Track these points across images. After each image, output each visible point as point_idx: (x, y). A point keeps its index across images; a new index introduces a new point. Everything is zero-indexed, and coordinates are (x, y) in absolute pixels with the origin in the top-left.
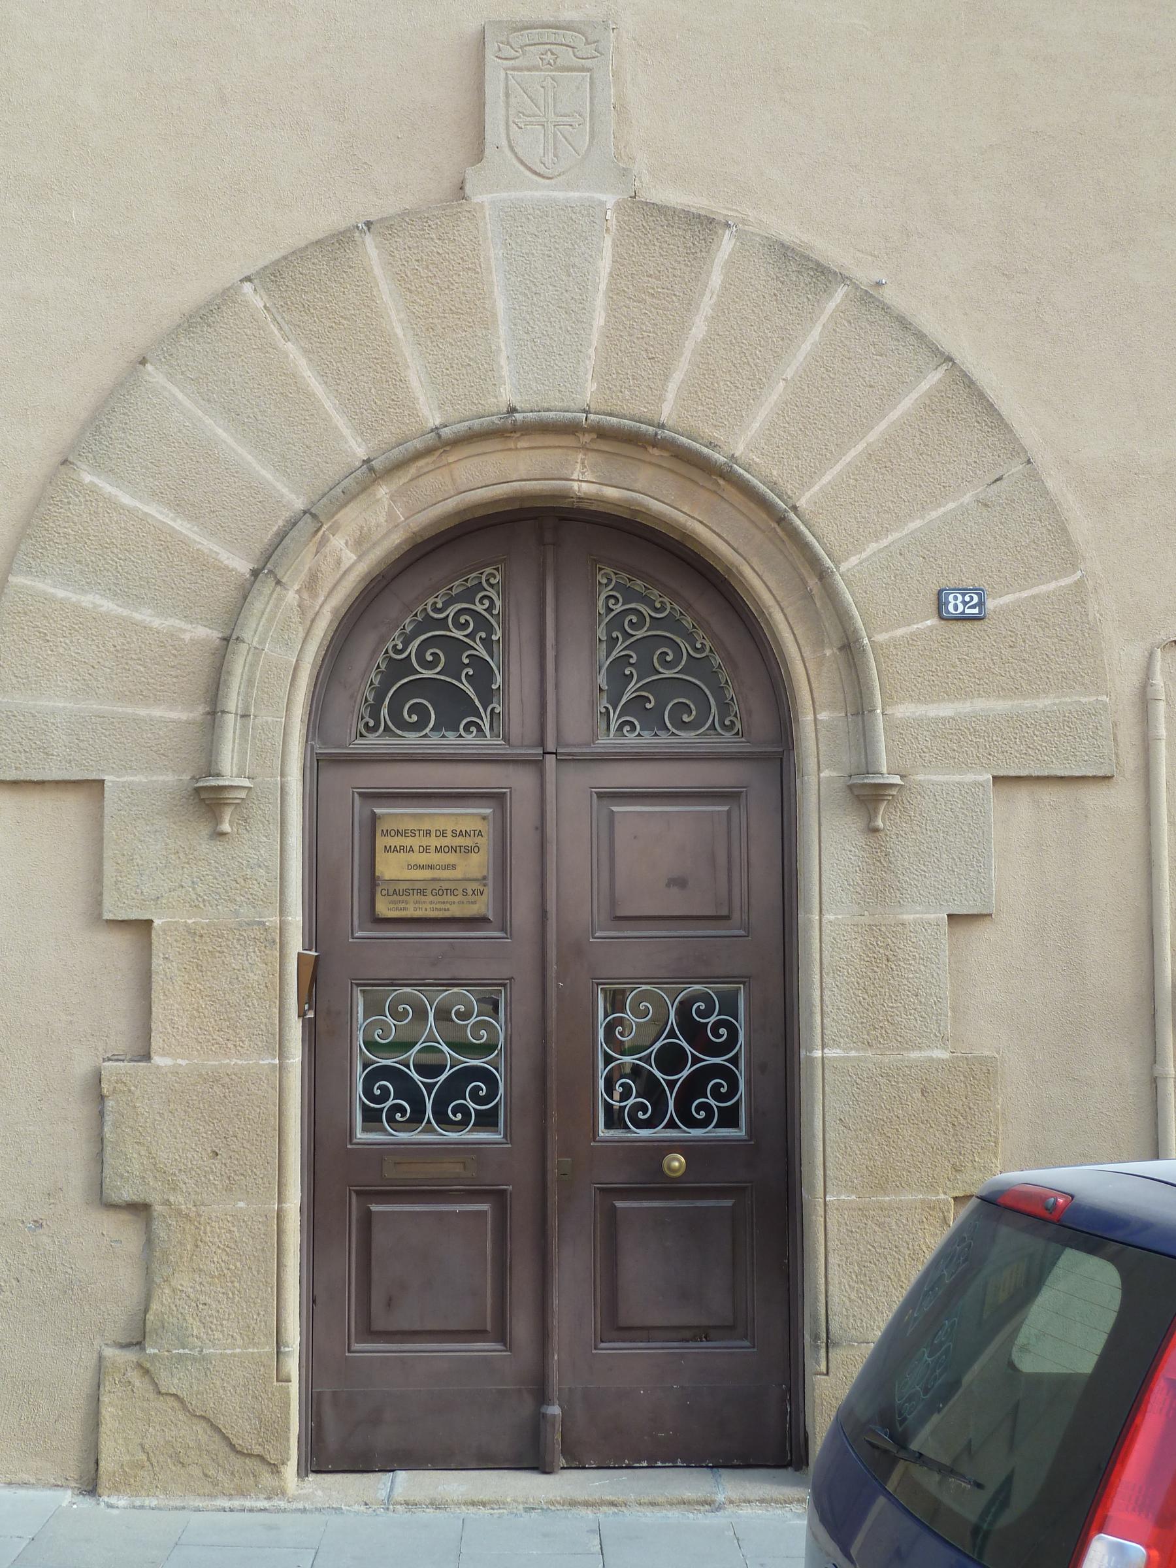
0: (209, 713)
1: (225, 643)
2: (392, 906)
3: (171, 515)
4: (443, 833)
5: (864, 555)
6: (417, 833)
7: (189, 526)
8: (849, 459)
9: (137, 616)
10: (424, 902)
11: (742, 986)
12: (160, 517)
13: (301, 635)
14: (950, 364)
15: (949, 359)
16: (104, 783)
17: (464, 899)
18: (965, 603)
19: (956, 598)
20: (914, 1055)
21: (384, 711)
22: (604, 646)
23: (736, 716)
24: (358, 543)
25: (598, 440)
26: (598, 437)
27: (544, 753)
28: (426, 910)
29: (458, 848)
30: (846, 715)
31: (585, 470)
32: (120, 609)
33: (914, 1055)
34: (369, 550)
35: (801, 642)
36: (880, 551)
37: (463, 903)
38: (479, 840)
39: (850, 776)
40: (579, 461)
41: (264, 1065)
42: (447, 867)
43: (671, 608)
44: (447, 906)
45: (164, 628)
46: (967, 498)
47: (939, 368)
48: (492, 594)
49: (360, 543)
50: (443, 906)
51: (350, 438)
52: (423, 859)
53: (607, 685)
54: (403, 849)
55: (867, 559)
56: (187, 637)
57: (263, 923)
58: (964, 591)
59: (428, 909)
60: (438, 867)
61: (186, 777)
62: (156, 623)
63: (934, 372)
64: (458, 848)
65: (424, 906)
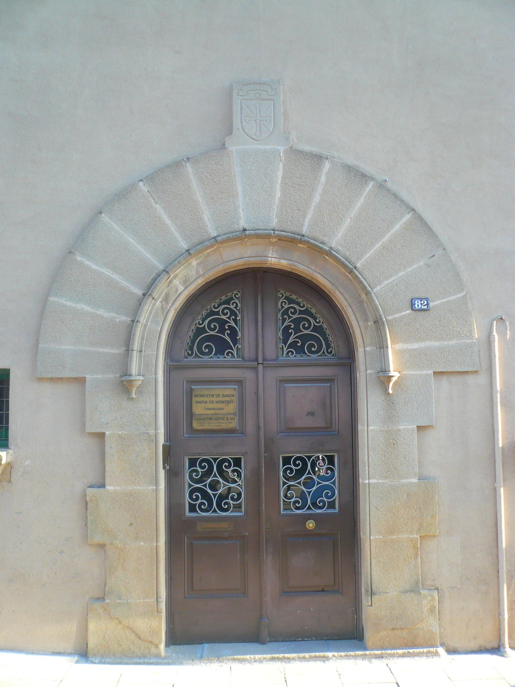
0: (126, 350)
4: (219, 396)
5: (382, 286)
7: (118, 277)
8: (376, 248)
9: (98, 312)
10: (212, 423)
12: (107, 273)
13: (163, 319)
14: (414, 211)
15: (413, 210)
18: (421, 304)
19: (418, 302)
20: (404, 481)
21: (195, 348)
23: (332, 348)
27: (258, 364)
28: (212, 426)
29: (225, 402)
30: (377, 349)
32: (92, 310)
33: (404, 481)
38: (233, 398)
39: (379, 372)
42: (220, 409)
44: (221, 424)
46: (421, 263)
48: (237, 301)
49: (186, 283)
50: (219, 424)
52: (211, 406)
56: (118, 320)
61: (118, 376)
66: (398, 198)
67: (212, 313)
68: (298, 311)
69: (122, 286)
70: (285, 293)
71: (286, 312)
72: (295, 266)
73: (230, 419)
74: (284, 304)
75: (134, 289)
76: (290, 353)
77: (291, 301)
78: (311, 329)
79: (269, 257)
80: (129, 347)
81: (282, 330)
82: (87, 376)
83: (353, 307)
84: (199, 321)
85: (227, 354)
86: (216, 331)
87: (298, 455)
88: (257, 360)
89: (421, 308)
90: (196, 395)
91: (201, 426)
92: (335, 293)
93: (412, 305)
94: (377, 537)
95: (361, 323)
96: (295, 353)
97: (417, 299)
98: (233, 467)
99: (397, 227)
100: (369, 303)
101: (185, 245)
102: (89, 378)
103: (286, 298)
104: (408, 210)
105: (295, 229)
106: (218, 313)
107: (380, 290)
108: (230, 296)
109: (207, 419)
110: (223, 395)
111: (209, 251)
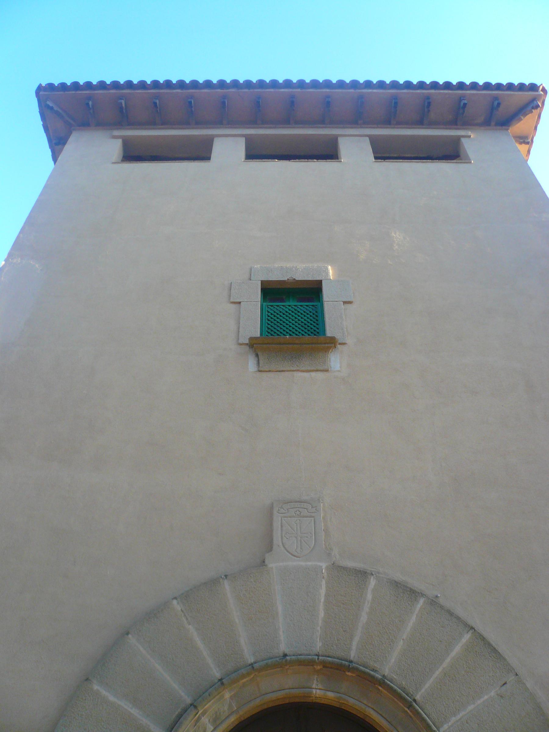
3: (130, 706)
12: (126, 707)
15: (472, 628)
36: (457, 721)
47: (469, 632)
55: (452, 726)
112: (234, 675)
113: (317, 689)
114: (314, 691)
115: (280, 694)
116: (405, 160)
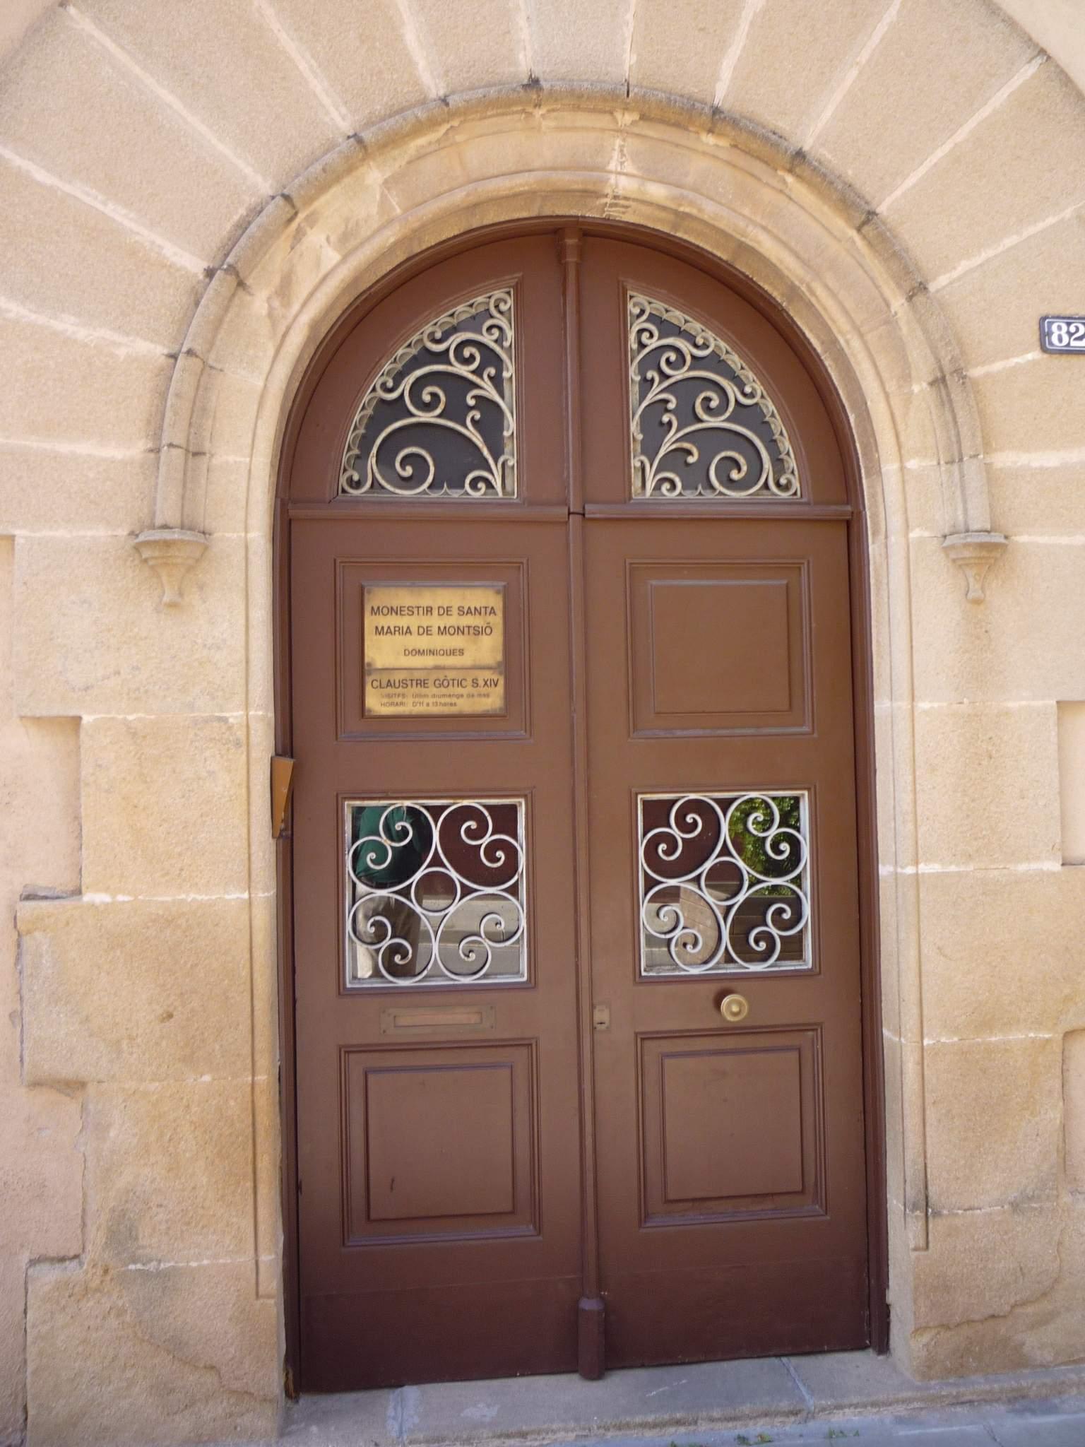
0: (151, 451)
1: (172, 361)
2: (385, 700)
3: (100, 197)
4: (447, 611)
5: (955, 274)
6: (415, 610)
7: (124, 211)
8: (935, 161)
9: (57, 325)
10: (426, 696)
11: (806, 793)
12: (88, 200)
13: (271, 352)
14: (1045, 58)
15: (1042, 52)
16: (13, 540)
17: (475, 691)
18: (1070, 334)
19: (1060, 328)
20: (1022, 867)
21: (372, 460)
22: (637, 388)
23: (793, 472)
24: (345, 237)
25: (641, 122)
26: (641, 119)
27: (569, 513)
28: (428, 705)
29: (466, 630)
30: (939, 464)
31: (624, 159)
32: (33, 316)
33: (1022, 867)
34: (356, 249)
35: (885, 375)
36: (972, 270)
37: (473, 696)
38: (491, 619)
39: (945, 537)
40: (617, 147)
41: (230, 900)
42: (452, 652)
43: (716, 346)
44: (454, 700)
45: (92, 341)
46: (1068, 213)
47: (1034, 62)
48: (503, 322)
49: (347, 240)
50: (448, 700)
51: (332, 109)
52: (423, 642)
53: (642, 431)
54: (398, 630)
55: (959, 278)
56: (122, 352)
57: (224, 720)
58: (1069, 320)
59: (431, 704)
60: (442, 652)
61: (123, 532)
62: (82, 334)
63: (1027, 66)
64: (466, 630)
65: (426, 700)
66: (999, 15)
67: (427, 356)
68: (688, 358)
69: (136, 242)
70: (650, 303)
71: (652, 360)
72: (691, 203)
73: (481, 683)
74: (646, 335)
75: (175, 254)
76: (666, 486)
77: (667, 328)
78: (727, 414)
79: (611, 172)
80: (160, 439)
81: (641, 416)
82: (17, 532)
83: (869, 337)
84: (347, 474)
85: (474, 484)
86: (438, 411)
87: (693, 796)
88: (565, 502)
89: (1068, 345)
90: (376, 609)
91: (392, 704)
92: (813, 293)
93: (1044, 335)
94: (943, 1040)
95: (891, 386)
96: (679, 485)
97: (1058, 317)
98: (493, 834)
99: (1000, 97)
100: (391, 700)
101: (343, 119)
102: (26, 538)
103: (652, 318)
104: (1029, 51)
105: (692, 89)
106: (442, 357)
107: (947, 286)
108: (482, 309)
109: (409, 683)
110: (460, 609)
111: (421, 141)
112: (392, 121)
113: (620, 173)
114: (613, 178)
115: (522, 182)
116: (793, 968)
